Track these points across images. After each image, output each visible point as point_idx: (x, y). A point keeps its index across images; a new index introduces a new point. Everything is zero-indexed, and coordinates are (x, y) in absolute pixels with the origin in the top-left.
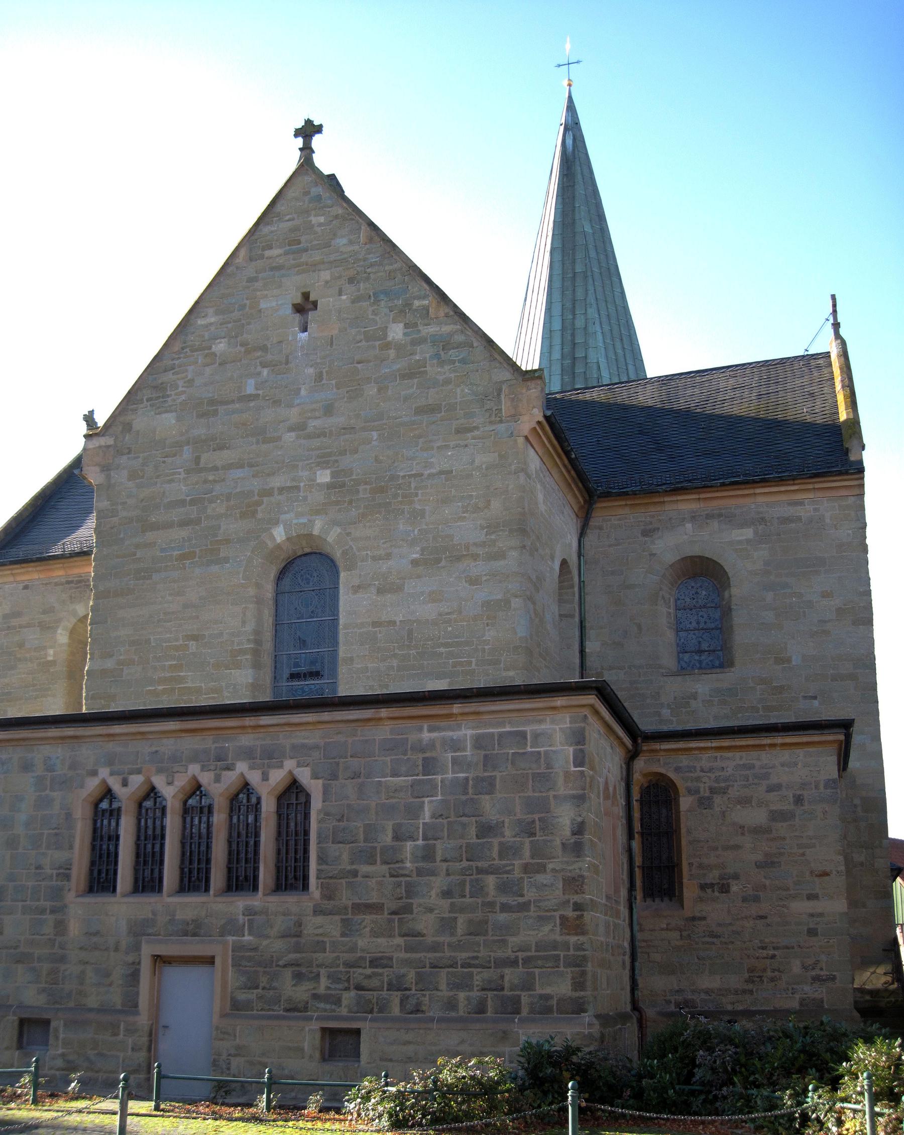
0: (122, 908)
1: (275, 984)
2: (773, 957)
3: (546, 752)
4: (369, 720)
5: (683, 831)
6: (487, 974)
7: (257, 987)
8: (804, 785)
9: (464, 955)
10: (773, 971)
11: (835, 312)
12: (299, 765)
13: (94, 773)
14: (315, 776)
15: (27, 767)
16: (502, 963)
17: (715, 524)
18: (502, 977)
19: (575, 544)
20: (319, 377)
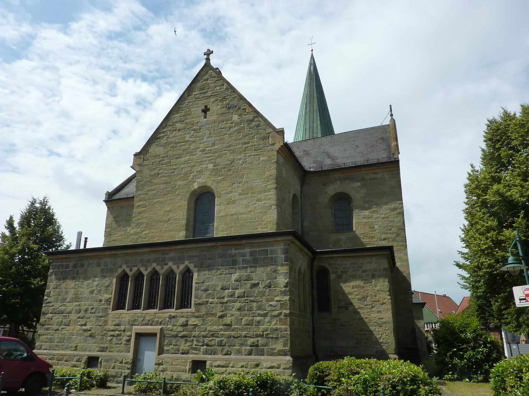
0: (126, 314)
1: (178, 344)
2: (365, 334)
3: (275, 257)
4: (214, 246)
5: (332, 287)
7: (171, 345)
8: (375, 270)
9: (244, 333)
10: (366, 340)
11: (391, 110)
12: (190, 263)
13: (121, 267)
14: (195, 267)
15: (98, 265)
16: (257, 336)
17: (347, 181)
18: (258, 341)
19: (299, 189)
20: (210, 134)
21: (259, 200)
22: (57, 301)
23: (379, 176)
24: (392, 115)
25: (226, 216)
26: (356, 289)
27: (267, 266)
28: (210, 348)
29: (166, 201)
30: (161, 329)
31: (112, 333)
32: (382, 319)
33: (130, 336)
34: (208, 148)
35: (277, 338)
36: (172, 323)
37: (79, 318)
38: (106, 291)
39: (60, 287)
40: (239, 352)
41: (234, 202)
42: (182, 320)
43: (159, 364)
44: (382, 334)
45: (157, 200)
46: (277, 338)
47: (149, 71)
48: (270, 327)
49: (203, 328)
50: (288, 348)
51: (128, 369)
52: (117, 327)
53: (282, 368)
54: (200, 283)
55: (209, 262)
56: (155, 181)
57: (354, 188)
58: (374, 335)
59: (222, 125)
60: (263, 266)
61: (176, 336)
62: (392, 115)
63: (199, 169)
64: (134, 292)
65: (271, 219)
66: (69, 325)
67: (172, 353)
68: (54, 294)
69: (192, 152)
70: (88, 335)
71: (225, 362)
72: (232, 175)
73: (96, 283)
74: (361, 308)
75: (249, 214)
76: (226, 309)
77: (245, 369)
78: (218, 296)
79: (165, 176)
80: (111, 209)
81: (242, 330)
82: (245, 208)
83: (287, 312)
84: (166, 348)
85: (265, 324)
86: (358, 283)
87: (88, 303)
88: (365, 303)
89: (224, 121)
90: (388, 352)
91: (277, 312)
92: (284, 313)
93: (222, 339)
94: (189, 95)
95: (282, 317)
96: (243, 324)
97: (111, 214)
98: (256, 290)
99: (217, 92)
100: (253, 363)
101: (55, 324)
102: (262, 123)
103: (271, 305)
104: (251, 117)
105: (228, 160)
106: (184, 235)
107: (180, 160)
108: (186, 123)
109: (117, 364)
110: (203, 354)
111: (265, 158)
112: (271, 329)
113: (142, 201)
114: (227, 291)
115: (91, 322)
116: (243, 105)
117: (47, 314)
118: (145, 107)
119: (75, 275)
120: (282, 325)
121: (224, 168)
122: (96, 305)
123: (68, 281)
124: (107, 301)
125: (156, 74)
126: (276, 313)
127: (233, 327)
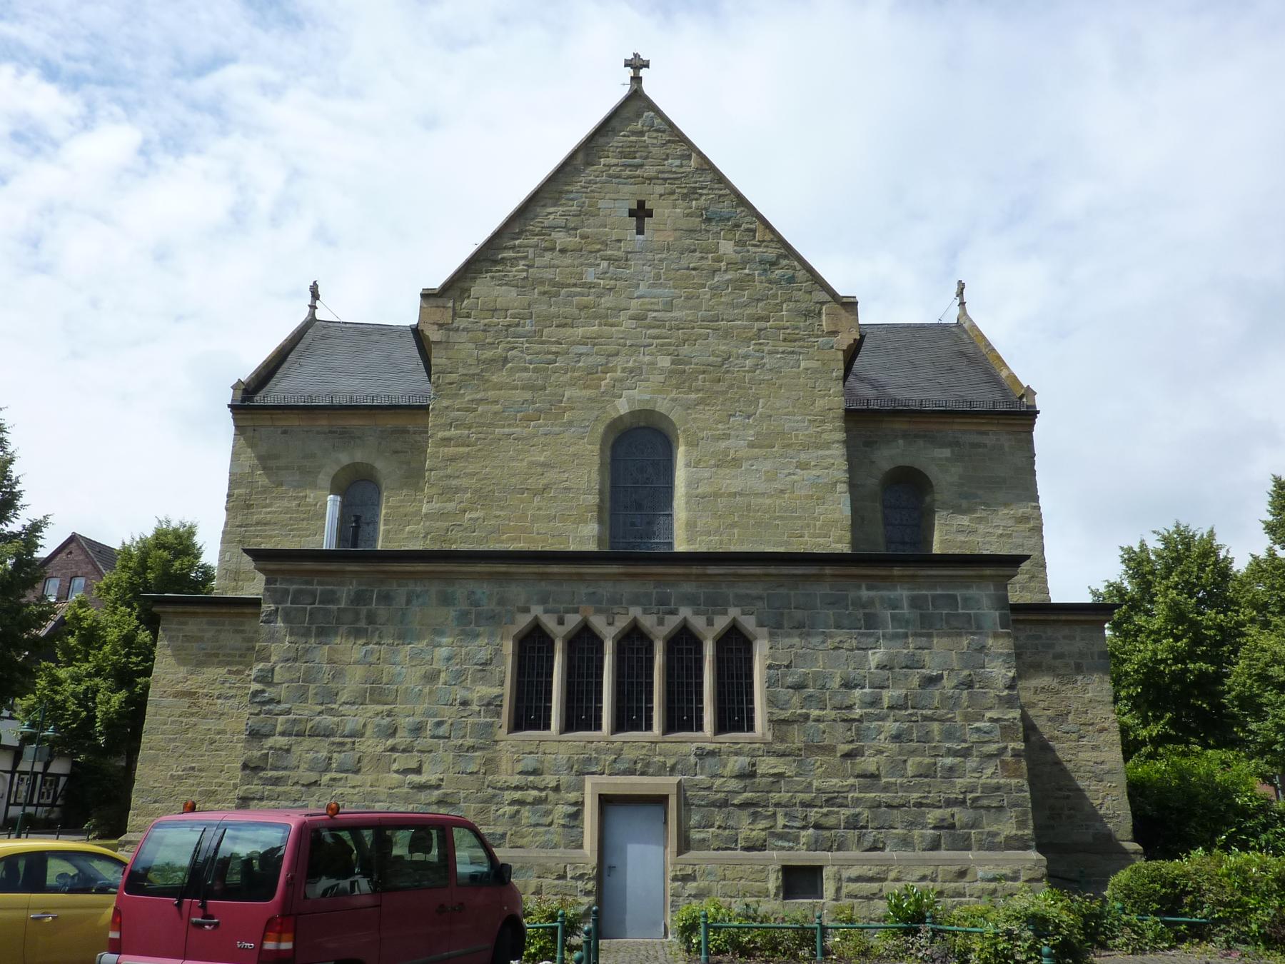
0: (555, 743)
1: (730, 823)
2: (1068, 797)
4: (814, 575)
6: (938, 813)
7: (712, 826)
9: (915, 795)
12: (744, 613)
13: (527, 610)
15: (446, 600)
17: (921, 443)
18: (953, 815)
20: (658, 277)
21: (803, 466)
22: (303, 698)
23: (990, 440)
24: (962, 304)
25: (716, 495)
26: (1042, 696)
27: (960, 635)
28: (826, 833)
29: (535, 436)
30: (679, 783)
31: (518, 795)
32: (1102, 763)
33: (580, 804)
34: (654, 314)
35: (1000, 808)
36: (707, 770)
37: (393, 749)
38: (480, 675)
39: (309, 656)
40: (906, 843)
41: (736, 463)
42: (737, 763)
43: (685, 879)
44: (1104, 798)
45: (506, 430)
46: (1000, 808)
47: (68, 57)
48: (982, 781)
49: (799, 783)
50: (1028, 832)
51: (588, 893)
52: (531, 778)
53: (1023, 878)
54: (779, 667)
55: (799, 614)
56: (495, 378)
57: (936, 461)
58: (1085, 798)
59: (693, 260)
60: (949, 635)
61: (724, 804)
62: (962, 304)
63: (630, 364)
64: (518, 682)
65: (837, 516)
66: (357, 771)
67: (718, 849)
68: (287, 676)
69: (607, 316)
70: (434, 799)
71: (876, 869)
72: (727, 392)
73: (443, 652)
74: (1057, 738)
75: (778, 497)
76: (860, 736)
77: (931, 885)
78: (837, 700)
79: (526, 370)
80: (250, 433)
81: (908, 789)
82: (768, 480)
83: (1021, 746)
84: (696, 835)
85: (968, 775)
86: (1045, 681)
87: (420, 708)
88: (1065, 727)
89: (694, 251)
90: (1118, 836)
91: (995, 746)
92: (1013, 749)
93: (858, 810)
94: (589, 164)
95: (1008, 757)
96: (910, 774)
97: (252, 445)
98: (937, 693)
99: (670, 172)
100: (949, 868)
101: (303, 766)
102: (801, 274)
103: (978, 730)
104: (771, 253)
105: (713, 353)
106: (595, 532)
107: (569, 331)
108: (582, 237)
109: (545, 882)
110: (808, 849)
111: (813, 364)
112: (985, 787)
113: (457, 427)
114: (857, 692)
115: (434, 762)
116: (746, 220)
117: (267, 736)
118: (37, 150)
119: (363, 624)
120: (1008, 777)
121: (704, 372)
122: (449, 714)
123: (338, 640)
124: (489, 704)
125: (87, 67)
126: (992, 748)
127: (884, 780)
